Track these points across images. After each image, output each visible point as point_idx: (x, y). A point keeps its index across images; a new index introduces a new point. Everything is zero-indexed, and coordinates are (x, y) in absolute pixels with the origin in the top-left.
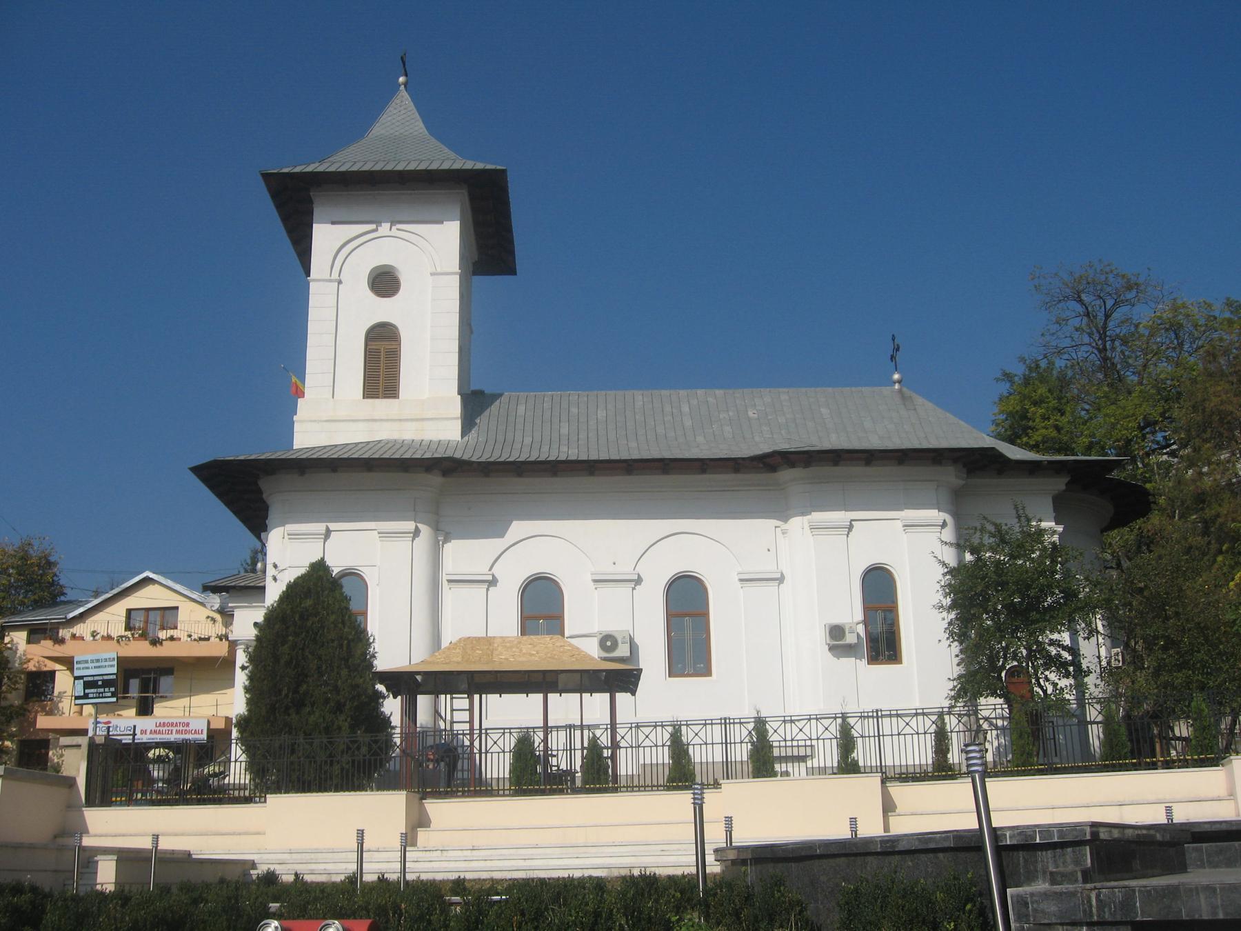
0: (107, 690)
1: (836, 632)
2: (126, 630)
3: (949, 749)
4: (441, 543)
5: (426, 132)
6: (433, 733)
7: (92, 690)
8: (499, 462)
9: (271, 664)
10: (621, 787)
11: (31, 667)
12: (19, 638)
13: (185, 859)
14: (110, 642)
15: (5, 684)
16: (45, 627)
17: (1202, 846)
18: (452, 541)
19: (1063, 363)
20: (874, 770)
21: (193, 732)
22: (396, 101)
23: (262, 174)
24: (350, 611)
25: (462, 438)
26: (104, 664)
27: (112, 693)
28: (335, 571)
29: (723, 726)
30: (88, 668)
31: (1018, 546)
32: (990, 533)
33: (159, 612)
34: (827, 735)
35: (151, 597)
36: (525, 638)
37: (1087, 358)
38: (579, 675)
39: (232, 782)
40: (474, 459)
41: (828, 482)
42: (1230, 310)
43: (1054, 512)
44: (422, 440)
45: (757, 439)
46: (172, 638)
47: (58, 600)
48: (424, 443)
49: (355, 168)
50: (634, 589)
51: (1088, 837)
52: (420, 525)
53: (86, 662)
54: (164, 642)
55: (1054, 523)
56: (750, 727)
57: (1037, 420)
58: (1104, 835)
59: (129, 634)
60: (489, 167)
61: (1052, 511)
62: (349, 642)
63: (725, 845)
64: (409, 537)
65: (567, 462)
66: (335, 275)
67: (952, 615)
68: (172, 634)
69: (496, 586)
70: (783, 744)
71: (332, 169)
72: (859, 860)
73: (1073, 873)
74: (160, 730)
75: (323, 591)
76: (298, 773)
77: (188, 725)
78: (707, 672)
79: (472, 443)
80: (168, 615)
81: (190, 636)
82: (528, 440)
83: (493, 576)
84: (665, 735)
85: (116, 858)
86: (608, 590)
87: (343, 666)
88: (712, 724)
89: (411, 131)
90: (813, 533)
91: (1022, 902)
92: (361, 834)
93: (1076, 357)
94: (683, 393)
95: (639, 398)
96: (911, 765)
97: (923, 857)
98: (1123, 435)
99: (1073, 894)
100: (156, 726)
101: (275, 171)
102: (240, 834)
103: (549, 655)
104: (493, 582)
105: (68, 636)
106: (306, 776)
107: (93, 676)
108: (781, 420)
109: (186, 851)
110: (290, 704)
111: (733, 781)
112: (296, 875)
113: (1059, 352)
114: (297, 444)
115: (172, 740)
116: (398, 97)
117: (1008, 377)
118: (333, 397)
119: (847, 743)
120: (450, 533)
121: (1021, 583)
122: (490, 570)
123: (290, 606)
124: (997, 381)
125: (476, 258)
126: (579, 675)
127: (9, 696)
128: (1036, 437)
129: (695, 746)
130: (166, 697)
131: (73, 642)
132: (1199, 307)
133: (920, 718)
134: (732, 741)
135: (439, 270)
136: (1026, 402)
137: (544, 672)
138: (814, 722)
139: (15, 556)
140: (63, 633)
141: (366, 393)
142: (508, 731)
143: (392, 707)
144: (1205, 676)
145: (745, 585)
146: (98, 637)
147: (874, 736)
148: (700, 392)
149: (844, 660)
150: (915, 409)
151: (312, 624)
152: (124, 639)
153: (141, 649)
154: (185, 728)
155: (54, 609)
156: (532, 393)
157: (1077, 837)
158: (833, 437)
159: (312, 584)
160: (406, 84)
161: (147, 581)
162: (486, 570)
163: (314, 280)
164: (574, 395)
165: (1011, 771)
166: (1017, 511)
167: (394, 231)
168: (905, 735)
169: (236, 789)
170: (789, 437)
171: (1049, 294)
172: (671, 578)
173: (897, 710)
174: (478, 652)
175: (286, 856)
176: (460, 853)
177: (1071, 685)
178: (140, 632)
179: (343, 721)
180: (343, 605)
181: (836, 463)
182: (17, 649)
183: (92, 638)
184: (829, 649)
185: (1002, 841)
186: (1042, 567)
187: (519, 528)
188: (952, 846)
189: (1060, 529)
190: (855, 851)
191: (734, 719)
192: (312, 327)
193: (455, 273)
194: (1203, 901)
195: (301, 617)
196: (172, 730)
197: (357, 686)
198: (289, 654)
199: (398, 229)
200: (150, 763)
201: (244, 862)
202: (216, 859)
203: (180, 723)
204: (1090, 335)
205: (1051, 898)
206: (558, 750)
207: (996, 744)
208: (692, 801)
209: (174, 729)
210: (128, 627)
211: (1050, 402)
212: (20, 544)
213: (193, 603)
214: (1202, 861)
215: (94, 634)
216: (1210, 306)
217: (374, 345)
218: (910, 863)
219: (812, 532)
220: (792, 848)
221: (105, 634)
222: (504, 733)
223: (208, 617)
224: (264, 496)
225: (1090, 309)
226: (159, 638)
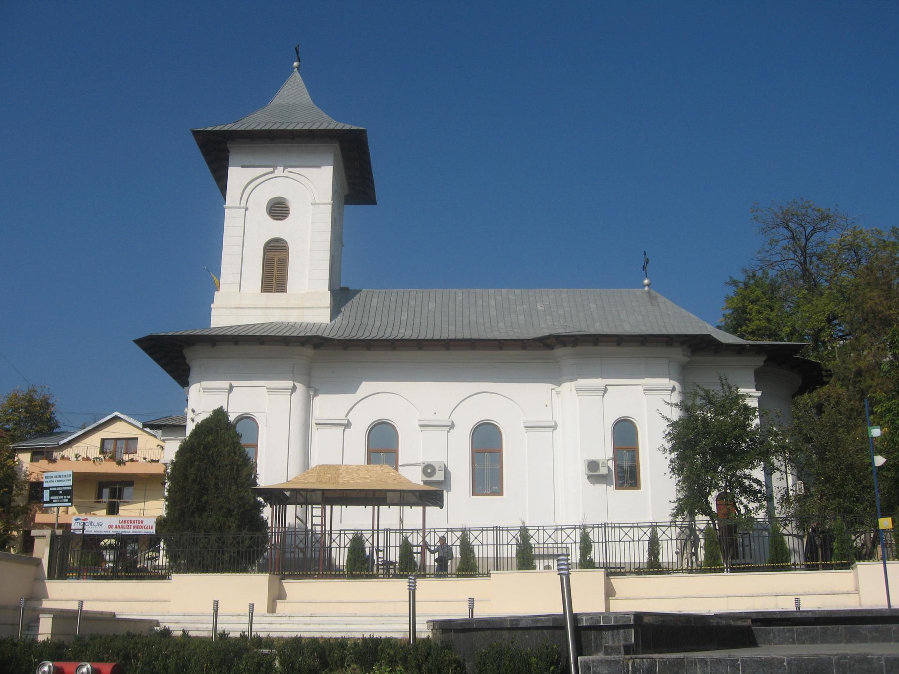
0: (65, 497)
1: (593, 465)
2: (100, 454)
3: (659, 553)
4: (311, 396)
5: (312, 102)
7: (56, 497)
8: (404, 339)
9: (182, 481)
11: (33, 479)
12: (24, 458)
13: (111, 618)
14: (88, 462)
16: (43, 450)
17: (793, 628)
18: (320, 395)
19: (775, 273)
20: (602, 566)
21: (146, 527)
22: (290, 81)
23: (193, 132)
24: (240, 444)
25: (331, 321)
27: (69, 499)
28: (232, 418)
29: (495, 531)
30: (53, 481)
31: (720, 406)
32: (701, 396)
33: (124, 441)
35: (119, 430)
36: (370, 467)
37: (793, 269)
38: (399, 493)
39: (160, 564)
40: (336, 337)
42: (894, 236)
43: (755, 381)
44: (302, 323)
45: (542, 325)
46: (132, 460)
47: (55, 431)
48: (303, 325)
49: (258, 128)
50: (448, 432)
51: (632, 622)
52: (296, 384)
53: (52, 477)
54: (126, 463)
55: (755, 390)
57: (753, 314)
58: (646, 620)
59: (102, 456)
60: (347, 127)
61: (754, 381)
62: (238, 466)
63: (468, 617)
64: (289, 392)
65: (402, 341)
66: (243, 204)
67: (674, 455)
68: (132, 457)
69: (350, 428)
71: (242, 128)
72: (498, 632)
73: (619, 647)
74: (122, 526)
75: (221, 430)
76: (199, 559)
77: (142, 522)
78: (499, 492)
79: (337, 325)
80: (130, 443)
81: (145, 459)
82: (377, 324)
83: (348, 421)
87: (233, 484)
88: (487, 530)
89: (300, 101)
90: (578, 394)
91: (587, 667)
92: (216, 603)
93: (783, 268)
94: (491, 291)
95: (460, 294)
96: (597, 563)
97: (535, 632)
98: (814, 325)
99: (617, 662)
100: (120, 523)
101: (202, 129)
103: (378, 479)
104: (348, 425)
105: (59, 457)
106: (205, 561)
107: (56, 487)
108: (561, 312)
109: (112, 612)
110: (195, 510)
111: (502, 572)
112: (184, 631)
113: (772, 264)
114: (213, 324)
115: (131, 533)
116: (293, 76)
117: (734, 283)
118: (240, 291)
119: (586, 545)
120: (318, 390)
121: (719, 433)
122: (346, 417)
123: (197, 440)
125: (347, 192)
126: (399, 493)
127: (16, 498)
128: (752, 327)
129: (513, 546)
130: (128, 502)
131: (62, 461)
132: (872, 234)
133: (636, 529)
134: (501, 543)
135: (317, 201)
136: (746, 301)
137: (374, 491)
138: (505, 532)
139: (24, 399)
140: (57, 455)
142: (343, 532)
143: (267, 513)
144: (852, 503)
145: (529, 431)
146: (80, 458)
147: (609, 542)
148: (504, 291)
149: (598, 486)
150: (658, 306)
151: (213, 453)
152: (98, 460)
153: (110, 468)
154: (140, 524)
155: (51, 437)
156: (383, 290)
157: (625, 622)
158: (598, 325)
159: (213, 425)
160: (298, 68)
161: (116, 419)
162: (343, 416)
163: (227, 207)
164: (413, 292)
165: (705, 569)
166: (721, 381)
167: (286, 173)
168: (643, 541)
169: (163, 569)
170: (565, 325)
171: (765, 222)
172: (476, 425)
173: (638, 523)
174: (328, 475)
175: (308, 619)
176: (301, 619)
177: (756, 507)
178: (110, 455)
179: (233, 522)
180: (235, 440)
181: (596, 344)
183: (75, 459)
184: (588, 478)
185: (580, 624)
186: (736, 422)
187: (366, 387)
188: (551, 625)
189: (759, 394)
190: (495, 626)
191: (614, 524)
193: (329, 204)
194: (698, 669)
195: (205, 448)
196: (131, 526)
197: (243, 498)
198: (195, 474)
199: (289, 172)
200: (104, 549)
201: (150, 621)
202: (128, 619)
203: (136, 521)
204: (795, 252)
205: (605, 664)
208: (408, 587)
209: (133, 525)
210: (102, 451)
211: (763, 301)
212: (28, 391)
213: (150, 436)
214: (793, 638)
215: (77, 456)
216: (880, 233)
217: (270, 254)
218: (527, 637)
219: (577, 393)
220: (460, 623)
221: (85, 457)
222: (413, 533)
223: (158, 446)
224: (187, 361)
225: (795, 234)
226: (123, 460)
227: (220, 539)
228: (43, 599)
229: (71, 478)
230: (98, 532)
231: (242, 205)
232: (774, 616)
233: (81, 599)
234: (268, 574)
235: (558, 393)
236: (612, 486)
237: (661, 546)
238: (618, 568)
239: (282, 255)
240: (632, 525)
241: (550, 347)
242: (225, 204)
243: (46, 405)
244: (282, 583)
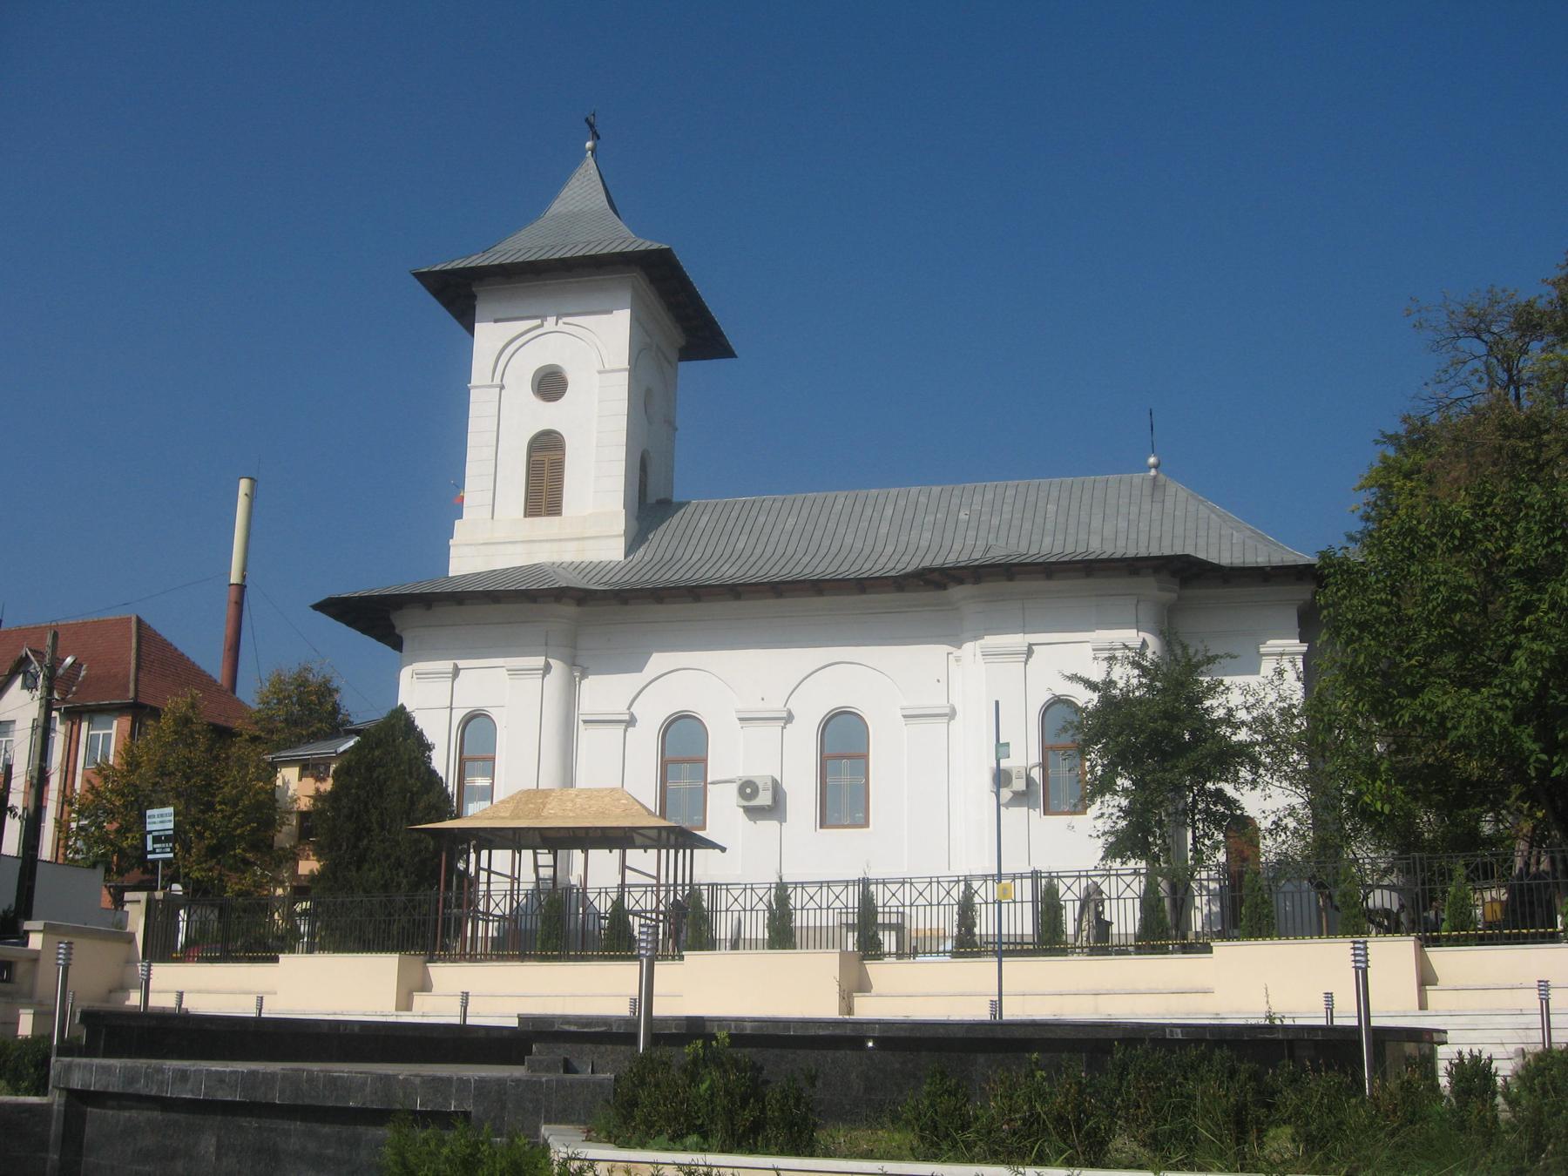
4: (577, 679)
15: (1260, 754)
22: (581, 171)
30: (155, 823)
34: (1129, 893)
41: (1003, 600)
50: (783, 728)
52: (550, 660)
55: (1298, 641)
60: (656, 246)
62: (413, 794)
66: (497, 381)
69: (635, 726)
83: (632, 715)
84: (852, 898)
85: (32, 1012)
95: (842, 499)
96: (1005, 935)
102: (159, 992)
104: (631, 722)
120: (588, 668)
124: (1377, 444)
138: (1113, 879)
141: (528, 510)
142: (725, 887)
160: (593, 150)
162: (624, 709)
182: (288, 788)
187: (659, 661)
192: (472, 439)
199: (565, 323)
207: (1206, 910)
217: (538, 456)
224: (397, 631)
228: (131, 990)
229: (172, 818)
231: (494, 383)
233: (180, 990)
234: (397, 955)
235: (958, 660)
236: (1038, 810)
237: (978, 913)
238: (1018, 943)
239: (553, 455)
240: (1077, 874)
242: (470, 383)
243: (326, 691)
244: (427, 967)
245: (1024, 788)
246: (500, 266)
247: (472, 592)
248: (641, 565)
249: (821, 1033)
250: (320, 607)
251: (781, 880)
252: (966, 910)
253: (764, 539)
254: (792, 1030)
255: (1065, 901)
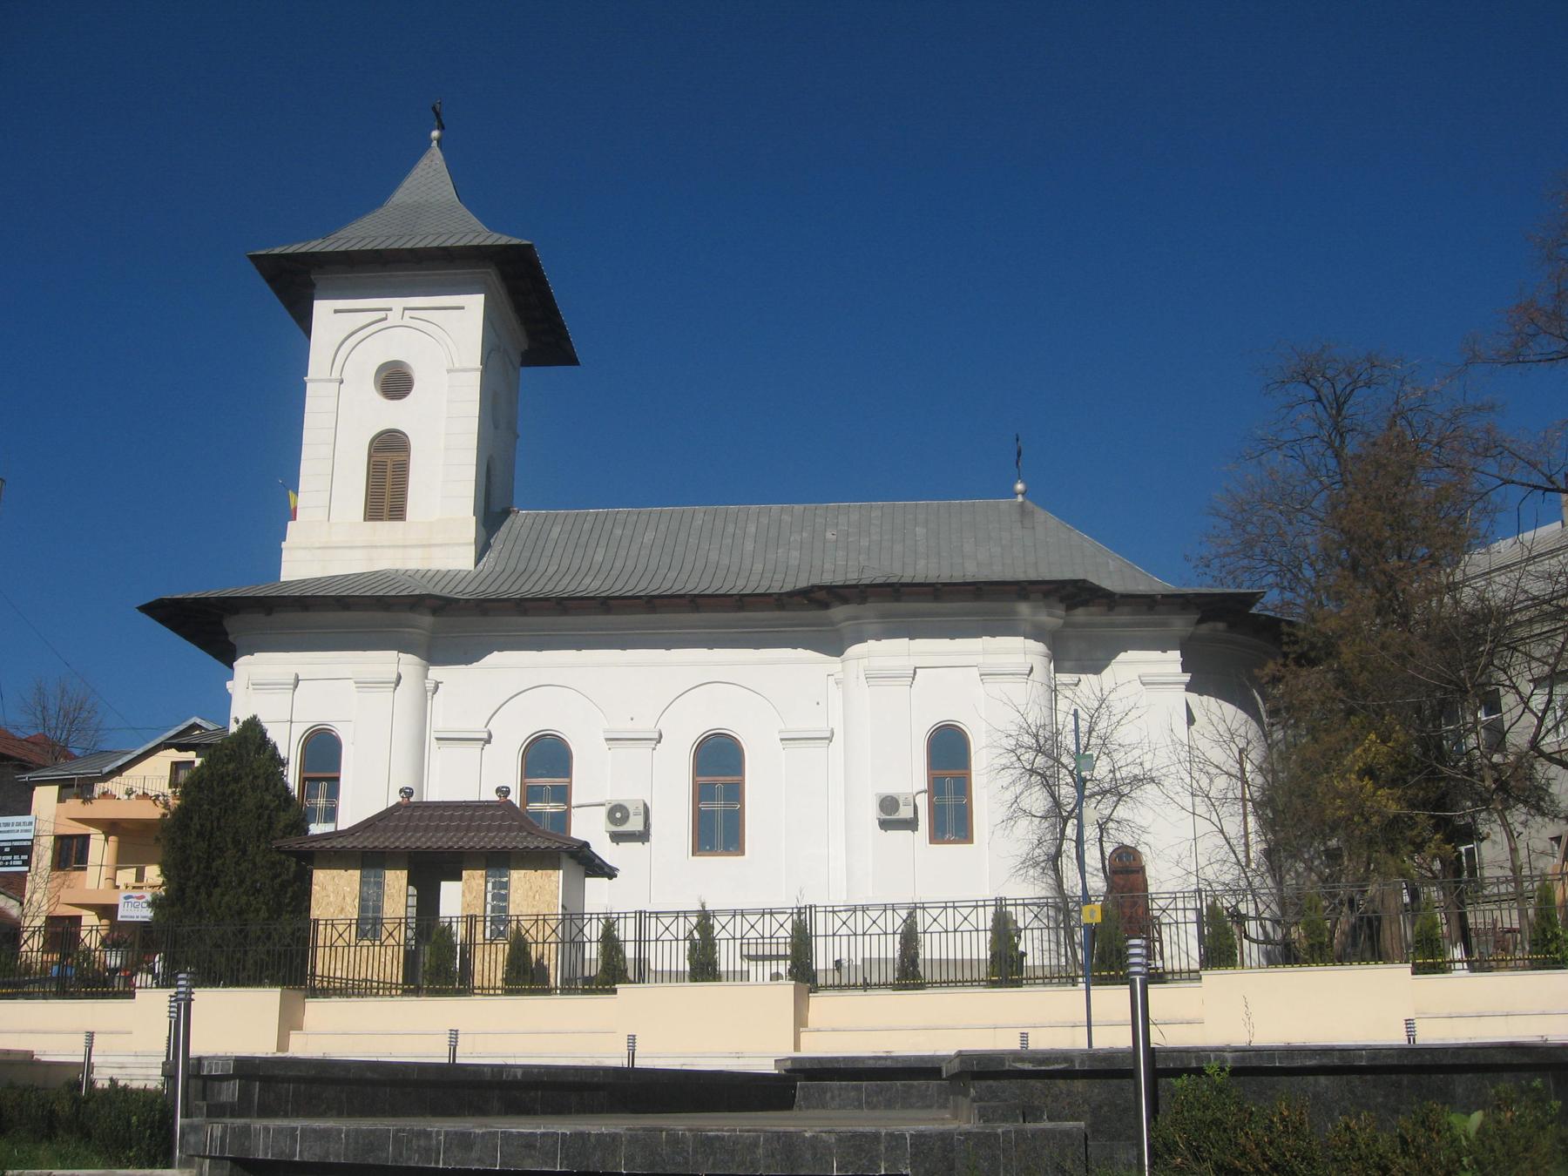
0: (16, 857)
1: (888, 803)
6: (483, 919)
10: (926, 983)
16: (72, 783)
22: (424, 163)
26: (15, 828)
56: (694, 920)
60: (515, 241)
66: (336, 375)
70: (760, 941)
78: (740, 850)
84: (986, 918)
86: (624, 752)
107: (12, 841)
108: (865, 542)
112: (111, 1079)
135: (457, 365)
138: (767, 917)
142: (596, 916)
145: (788, 746)
150: (1033, 528)
160: (439, 141)
163: (311, 381)
173: (1023, 899)
175: (132, 1059)
183: (126, 797)
193: (476, 370)
206: (484, 944)
214: (860, 1100)
215: (129, 793)
217: (380, 457)
222: (677, 917)
224: (231, 638)
227: (241, 931)
230: (126, 917)
232: (836, 1065)
233: (91, 1030)
234: (279, 989)
240: (944, 905)
241: (825, 605)
242: (307, 376)
245: (912, 816)
246: (346, 253)
247: (323, 596)
248: (494, 575)
249: (1308, 1064)
250: (149, 609)
251: (703, 906)
252: (910, 938)
253: (623, 553)
254: (1277, 1061)
255: (720, 940)
